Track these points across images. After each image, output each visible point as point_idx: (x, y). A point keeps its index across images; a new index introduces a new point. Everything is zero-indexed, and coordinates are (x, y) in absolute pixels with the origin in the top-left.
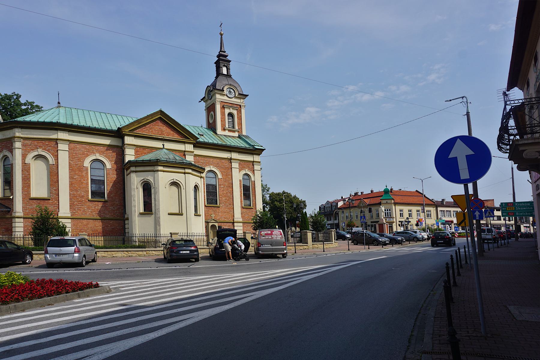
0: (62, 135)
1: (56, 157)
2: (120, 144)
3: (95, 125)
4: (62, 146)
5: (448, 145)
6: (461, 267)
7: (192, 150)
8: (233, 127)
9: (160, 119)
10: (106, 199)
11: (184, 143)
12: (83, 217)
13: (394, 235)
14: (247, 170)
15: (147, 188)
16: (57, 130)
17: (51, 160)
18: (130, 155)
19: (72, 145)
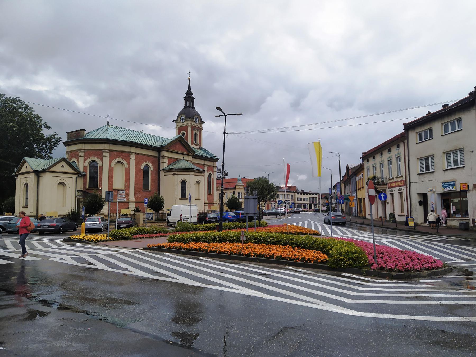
0: (133, 149)
1: (129, 163)
2: (157, 155)
3: (125, 139)
4: (133, 157)
5: (443, 185)
6: (185, 292)
7: (191, 160)
8: (196, 142)
9: (179, 141)
10: (150, 189)
11: (188, 155)
12: (140, 201)
13: (119, 228)
14: (120, 158)
15: (402, 211)
16: (130, 146)
17: (126, 165)
18: (165, 164)
19: (112, 152)
